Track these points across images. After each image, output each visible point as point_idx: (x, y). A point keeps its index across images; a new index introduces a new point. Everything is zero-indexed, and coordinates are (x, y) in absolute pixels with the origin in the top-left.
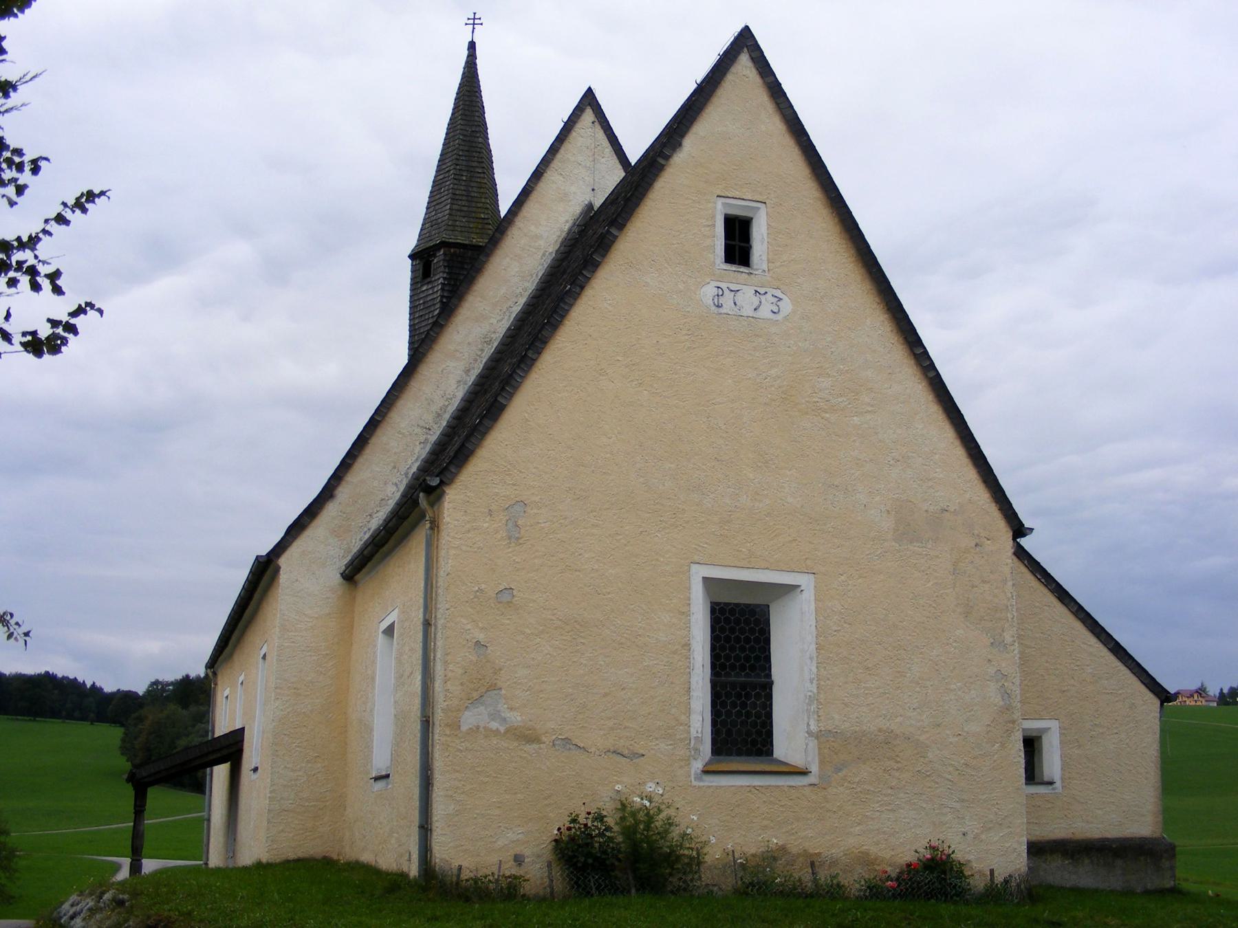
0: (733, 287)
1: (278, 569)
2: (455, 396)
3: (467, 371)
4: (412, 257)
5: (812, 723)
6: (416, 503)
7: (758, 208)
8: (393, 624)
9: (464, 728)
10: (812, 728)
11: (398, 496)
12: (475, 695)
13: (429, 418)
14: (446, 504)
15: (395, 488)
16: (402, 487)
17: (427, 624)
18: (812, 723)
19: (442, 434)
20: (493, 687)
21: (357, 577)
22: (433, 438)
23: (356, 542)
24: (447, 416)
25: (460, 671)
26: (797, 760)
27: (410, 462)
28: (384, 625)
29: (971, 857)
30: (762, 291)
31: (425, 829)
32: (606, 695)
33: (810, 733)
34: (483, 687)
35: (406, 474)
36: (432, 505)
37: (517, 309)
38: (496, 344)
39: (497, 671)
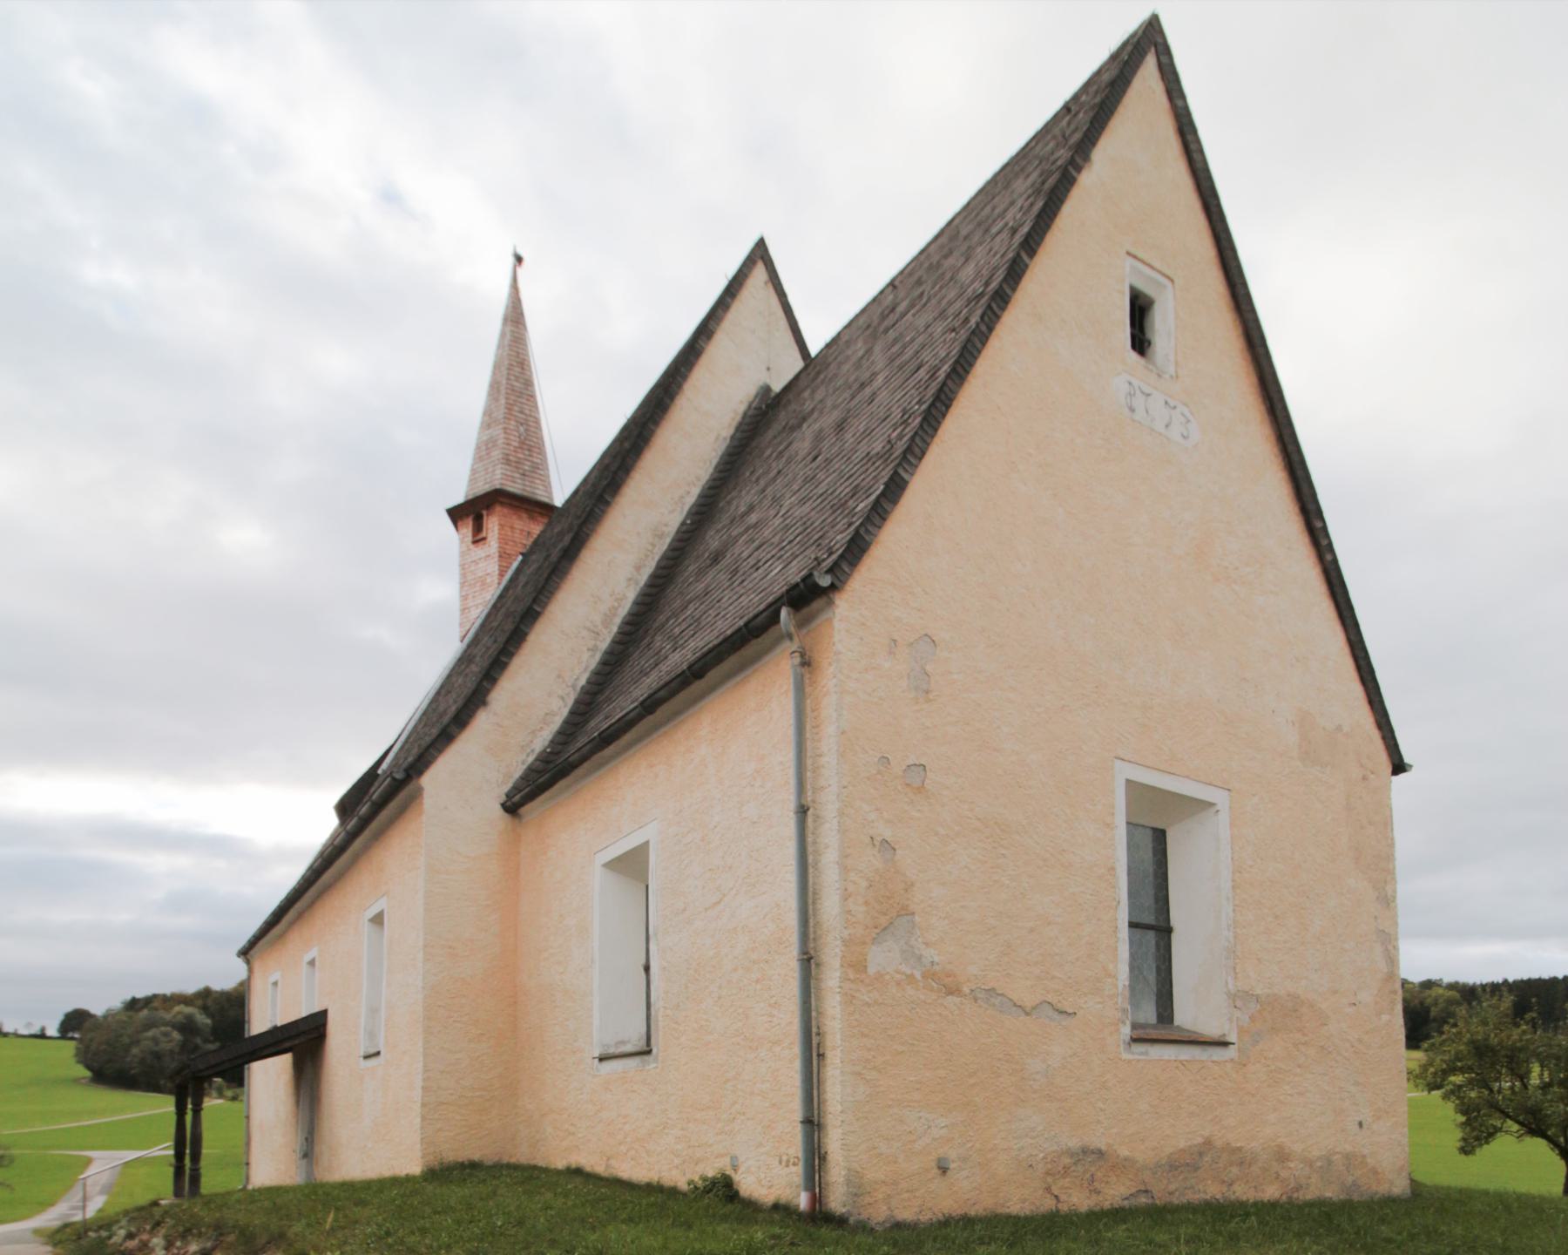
0: (1147, 389)
1: (418, 794)
2: (625, 597)
3: (638, 568)
4: (468, 515)
5: (1231, 982)
6: (774, 619)
7: (1165, 287)
8: (645, 847)
9: (871, 970)
10: (1230, 986)
11: (565, 712)
12: (883, 921)
13: (598, 619)
14: (837, 624)
15: (561, 703)
16: (570, 702)
17: (803, 811)
18: (1231, 982)
19: (614, 642)
20: (906, 911)
21: (523, 810)
22: (604, 644)
23: (516, 764)
24: (618, 621)
25: (864, 884)
26: (1211, 1030)
27: (577, 672)
28: (308, 958)
29: (1366, 1151)
30: (1172, 403)
31: (813, 1124)
32: (1032, 930)
33: (1228, 994)
34: (891, 912)
35: (574, 686)
36: (802, 624)
37: (691, 500)
38: (668, 540)
39: (909, 886)
